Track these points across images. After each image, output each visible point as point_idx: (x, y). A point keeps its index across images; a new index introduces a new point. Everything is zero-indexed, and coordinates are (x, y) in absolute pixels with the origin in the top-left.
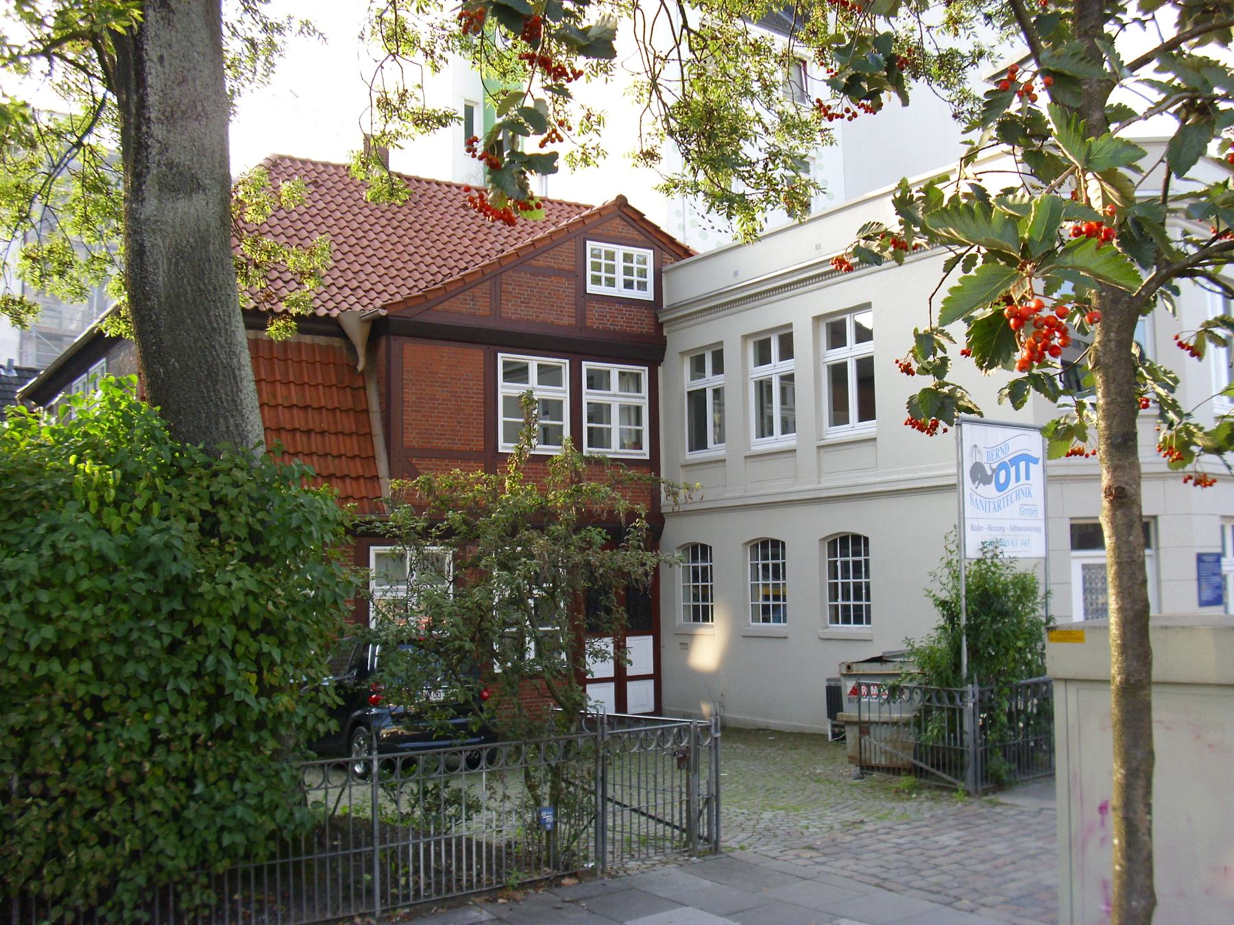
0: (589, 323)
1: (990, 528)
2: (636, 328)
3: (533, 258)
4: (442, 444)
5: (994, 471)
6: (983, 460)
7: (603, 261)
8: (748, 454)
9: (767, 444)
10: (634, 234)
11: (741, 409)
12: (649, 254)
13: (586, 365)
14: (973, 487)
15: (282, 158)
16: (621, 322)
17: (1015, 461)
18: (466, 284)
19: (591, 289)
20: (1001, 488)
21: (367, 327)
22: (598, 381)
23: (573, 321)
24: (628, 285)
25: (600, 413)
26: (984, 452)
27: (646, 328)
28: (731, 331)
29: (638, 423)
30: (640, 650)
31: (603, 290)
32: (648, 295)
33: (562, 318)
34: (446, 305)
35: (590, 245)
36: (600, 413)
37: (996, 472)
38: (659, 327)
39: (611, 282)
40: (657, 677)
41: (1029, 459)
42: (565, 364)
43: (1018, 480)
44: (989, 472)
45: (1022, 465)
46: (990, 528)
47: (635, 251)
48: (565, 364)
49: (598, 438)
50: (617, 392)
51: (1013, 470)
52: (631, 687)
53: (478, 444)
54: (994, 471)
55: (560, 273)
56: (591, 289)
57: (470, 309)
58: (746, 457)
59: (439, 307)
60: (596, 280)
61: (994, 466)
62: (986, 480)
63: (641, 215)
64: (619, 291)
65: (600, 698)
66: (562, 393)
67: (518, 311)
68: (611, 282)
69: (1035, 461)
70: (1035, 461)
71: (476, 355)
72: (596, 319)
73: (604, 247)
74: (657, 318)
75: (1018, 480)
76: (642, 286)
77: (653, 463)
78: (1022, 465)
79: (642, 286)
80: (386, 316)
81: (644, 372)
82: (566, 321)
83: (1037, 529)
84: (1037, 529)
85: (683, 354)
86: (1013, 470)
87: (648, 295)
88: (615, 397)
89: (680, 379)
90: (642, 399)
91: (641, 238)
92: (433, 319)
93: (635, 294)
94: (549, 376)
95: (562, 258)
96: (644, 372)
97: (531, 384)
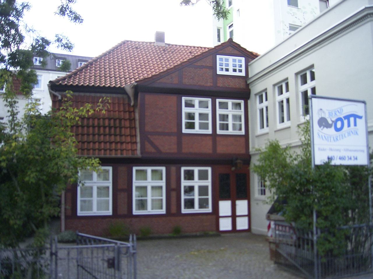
0: (218, 85)
1: (331, 150)
2: (237, 86)
3: (195, 62)
4: (160, 130)
5: (333, 122)
6: (327, 116)
7: (224, 62)
8: (275, 129)
9: (280, 126)
10: (236, 52)
11: (274, 114)
12: (243, 59)
13: (218, 101)
14: (320, 129)
15: (128, 41)
16: (232, 84)
17: (348, 117)
18: (168, 72)
19: (219, 72)
20: (337, 130)
21: (133, 90)
22: (224, 106)
23: (212, 84)
24: (235, 70)
25: (224, 117)
26: (327, 113)
27: (242, 86)
28: (268, 83)
29: (241, 121)
30: (242, 206)
31: (224, 73)
32: (243, 74)
33: (208, 84)
34: (161, 80)
35: (218, 57)
36: (224, 117)
37: (335, 122)
38: (248, 85)
39: (227, 70)
40: (249, 216)
41: (356, 117)
42: (209, 100)
43: (349, 125)
44: (330, 122)
45: (352, 119)
46: (331, 150)
47: (237, 58)
48: (209, 100)
49: (225, 127)
50: (231, 109)
51: (346, 122)
52: (238, 220)
53: (175, 130)
54: (333, 122)
55: (207, 67)
56: (219, 72)
57: (173, 82)
58: (275, 131)
59: (158, 81)
60: (222, 69)
61: (334, 119)
62: (328, 126)
63: (239, 45)
64: (231, 73)
65: (225, 225)
66: (209, 111)
67: (188, 82)
68: (227, 70)
69: (360, 117)
70: (360, 117)
71: (173, 98)
72: (220, 84)
73: (224, 57)
74: (246, 82)
75: (349, 125)
76: (240, 71)
77: (246, 136)
78: (352, 119)
79: (240, 71)
80: (137, 85)
81: (242, 102)
82: (209, 84)
83: (363, 151)
84: (363, 151)
85: (256, 95)
86: (346, 122)
87: (243, 74)
88: (230, 111)
89: (256, 105)
90: (241, 112)
91: (240, 53)
92: (156, 85)
93: (237, 74)
94: (202, 105)
95: (208, 62)
96: (242, 102)
97: (197, 108)
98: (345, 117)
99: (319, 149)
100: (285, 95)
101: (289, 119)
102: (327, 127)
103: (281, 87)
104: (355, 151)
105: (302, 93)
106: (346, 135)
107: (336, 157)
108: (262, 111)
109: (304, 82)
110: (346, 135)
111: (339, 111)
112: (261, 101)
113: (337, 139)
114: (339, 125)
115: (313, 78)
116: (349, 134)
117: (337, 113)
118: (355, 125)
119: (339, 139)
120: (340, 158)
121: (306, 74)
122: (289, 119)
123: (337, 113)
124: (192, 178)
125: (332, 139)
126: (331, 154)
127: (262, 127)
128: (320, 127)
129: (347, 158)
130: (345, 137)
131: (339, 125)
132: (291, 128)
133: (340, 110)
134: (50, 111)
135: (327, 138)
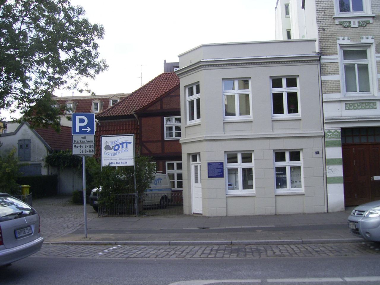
6: (110, 144)
17: (122, 144)
20: (115, 150)
44: (112, 147)
51: (121, 146)
62: (110, 149)
78: (125, 145)
86: (121, 146)
98: (120, 144)
99: (105, 160)
100: (195, 96)
101: (199, 117)
102: (110, 150)
103: (192, 88)
104: (126, 159)
105: (189, 102)
106: (121, 152)
107: (114, 163)
108: (191, 103)
109: (191, 94)
110: (121, 152)
111: (117, 141)
112: (191, 94)
113: (115, 154)
114: (117, 148)
115: (198, 92)
116: (122, 152)
117: (116, 142)
118: (127, 147)
119: (116, 154)
120: (116, 163)
121: (193, 87)
122: (199, 117)
123: (116, 142)
124: (179, 186)
125: (112, 155)
126: (111, 161)
127: (192, 118)
128: (106, 150)
129: (121, 163)
130: (120, 153)
131: (117, 148)
132: (201, 125)
133: (118, 140)
134: (378, 281)
135: (110, 154)
